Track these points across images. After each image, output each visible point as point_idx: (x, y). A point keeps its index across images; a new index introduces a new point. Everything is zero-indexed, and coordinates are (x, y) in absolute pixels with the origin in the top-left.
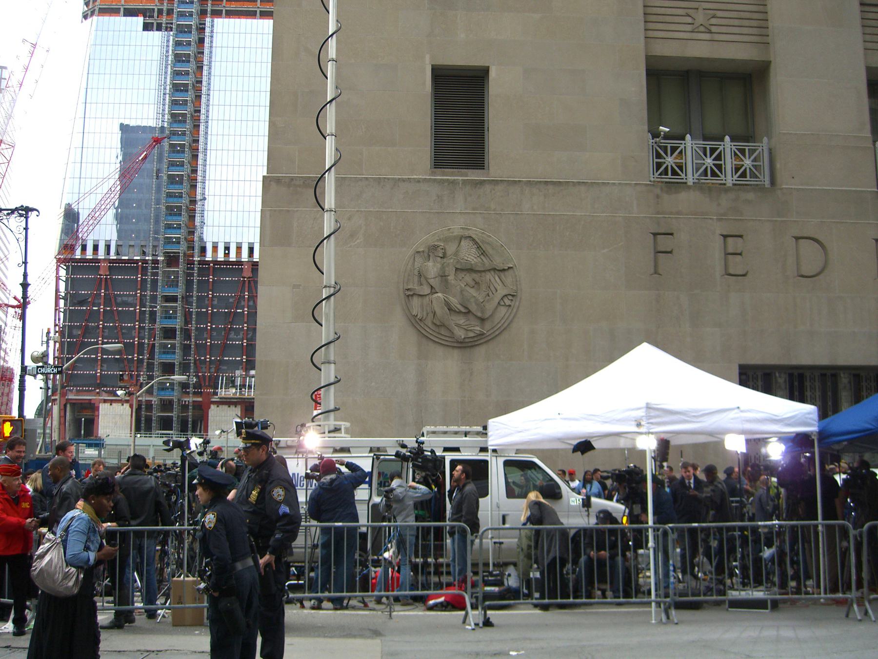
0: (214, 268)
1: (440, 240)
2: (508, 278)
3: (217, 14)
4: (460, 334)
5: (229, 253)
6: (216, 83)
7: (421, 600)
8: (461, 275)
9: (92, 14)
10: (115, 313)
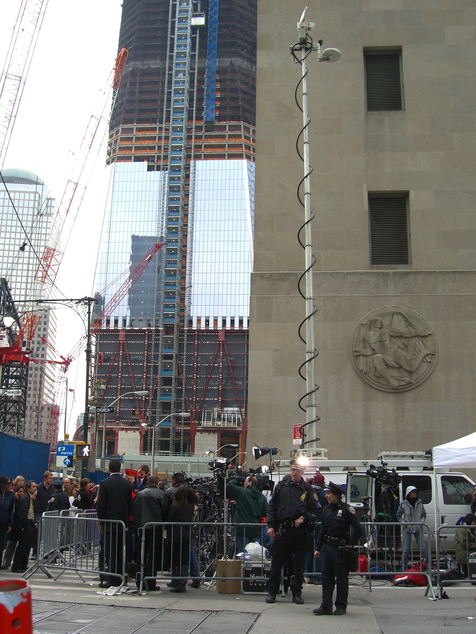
0: (198, 335)
1: (378, 316)
2: (429, 342)
3: (198, 157)
4: (394, 383)
5: (208, 324)
6: (198, 204)
7: (391, 578)
8: (394, 340)
9: (113, 161)
10: (130, 367)
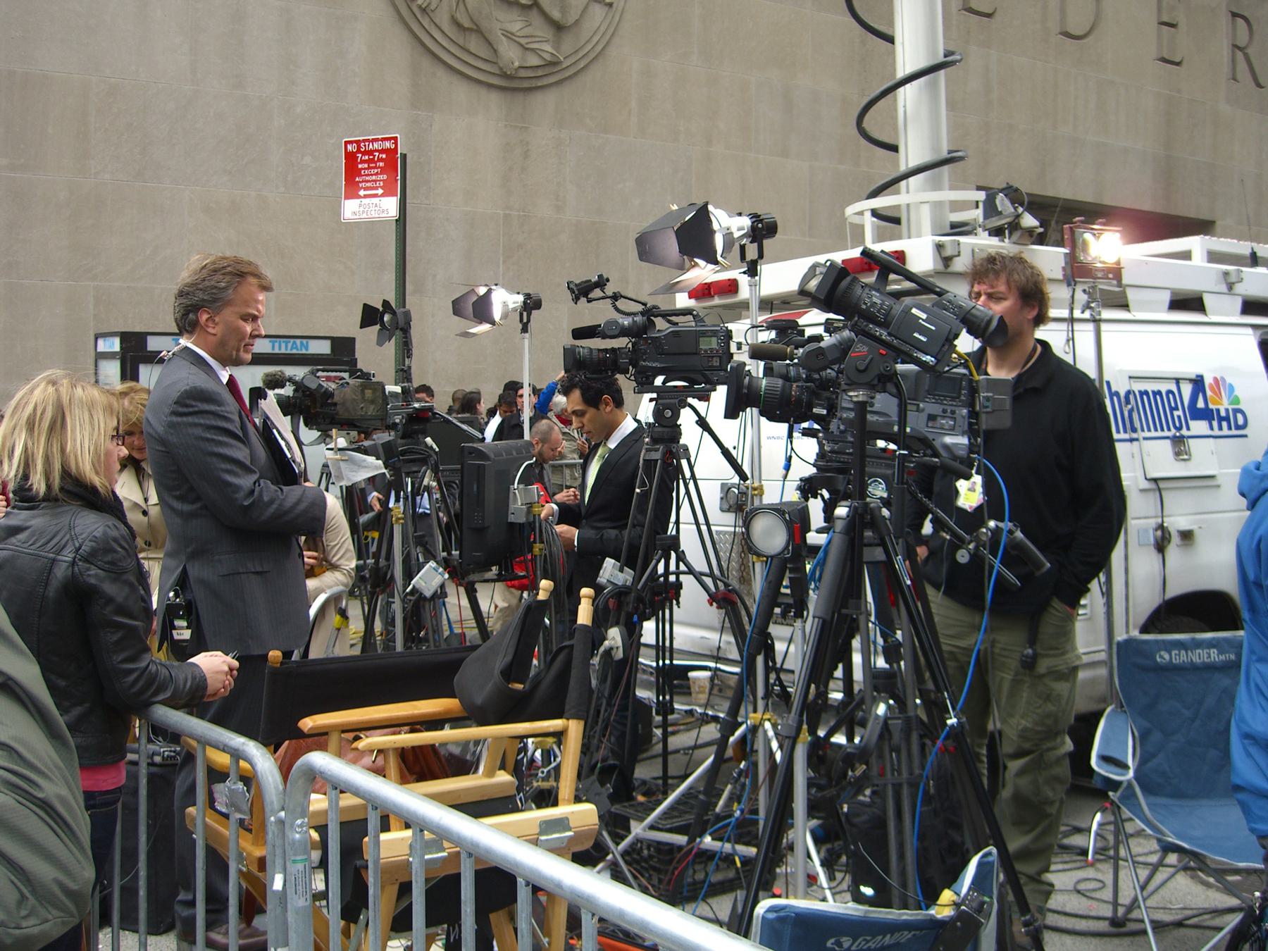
4: (511, 55)
